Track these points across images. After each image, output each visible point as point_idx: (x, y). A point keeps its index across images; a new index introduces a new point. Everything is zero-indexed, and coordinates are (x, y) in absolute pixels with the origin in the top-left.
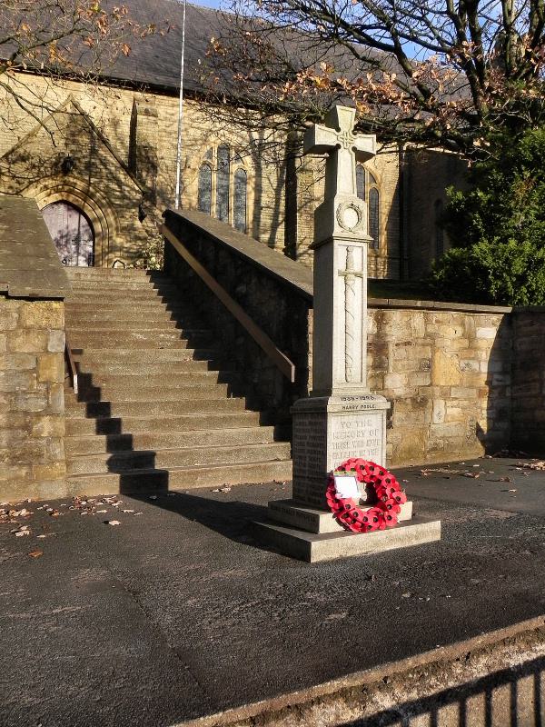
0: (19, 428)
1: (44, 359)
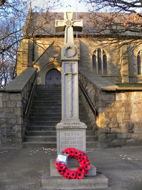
0: (9, 128)
1: (15, 109)
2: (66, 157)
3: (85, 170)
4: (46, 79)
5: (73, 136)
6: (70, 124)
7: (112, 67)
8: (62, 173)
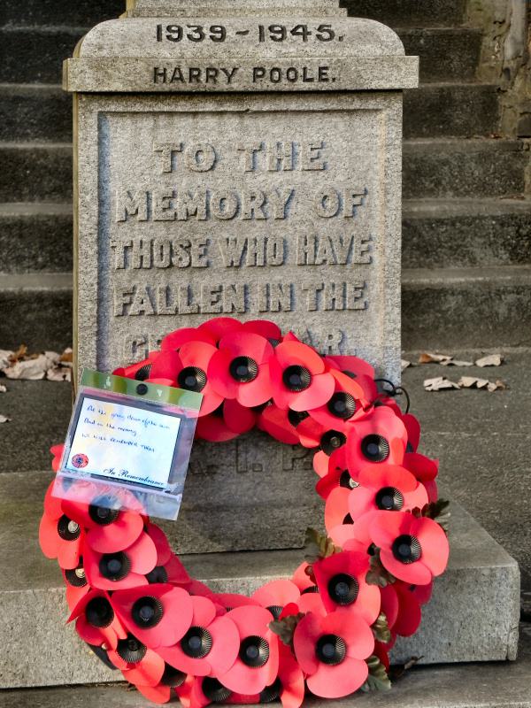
2: (174, 423)
3: (382, 590)
5: (258, 182)
6: (230, 33)
8: (115, 630)
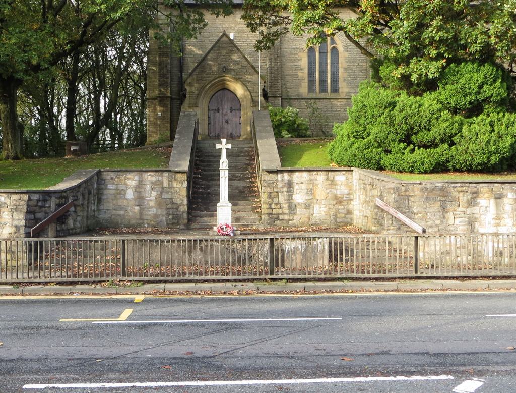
4: (209, 110)
7: (350, 76)
